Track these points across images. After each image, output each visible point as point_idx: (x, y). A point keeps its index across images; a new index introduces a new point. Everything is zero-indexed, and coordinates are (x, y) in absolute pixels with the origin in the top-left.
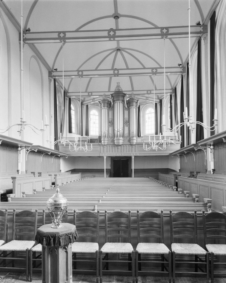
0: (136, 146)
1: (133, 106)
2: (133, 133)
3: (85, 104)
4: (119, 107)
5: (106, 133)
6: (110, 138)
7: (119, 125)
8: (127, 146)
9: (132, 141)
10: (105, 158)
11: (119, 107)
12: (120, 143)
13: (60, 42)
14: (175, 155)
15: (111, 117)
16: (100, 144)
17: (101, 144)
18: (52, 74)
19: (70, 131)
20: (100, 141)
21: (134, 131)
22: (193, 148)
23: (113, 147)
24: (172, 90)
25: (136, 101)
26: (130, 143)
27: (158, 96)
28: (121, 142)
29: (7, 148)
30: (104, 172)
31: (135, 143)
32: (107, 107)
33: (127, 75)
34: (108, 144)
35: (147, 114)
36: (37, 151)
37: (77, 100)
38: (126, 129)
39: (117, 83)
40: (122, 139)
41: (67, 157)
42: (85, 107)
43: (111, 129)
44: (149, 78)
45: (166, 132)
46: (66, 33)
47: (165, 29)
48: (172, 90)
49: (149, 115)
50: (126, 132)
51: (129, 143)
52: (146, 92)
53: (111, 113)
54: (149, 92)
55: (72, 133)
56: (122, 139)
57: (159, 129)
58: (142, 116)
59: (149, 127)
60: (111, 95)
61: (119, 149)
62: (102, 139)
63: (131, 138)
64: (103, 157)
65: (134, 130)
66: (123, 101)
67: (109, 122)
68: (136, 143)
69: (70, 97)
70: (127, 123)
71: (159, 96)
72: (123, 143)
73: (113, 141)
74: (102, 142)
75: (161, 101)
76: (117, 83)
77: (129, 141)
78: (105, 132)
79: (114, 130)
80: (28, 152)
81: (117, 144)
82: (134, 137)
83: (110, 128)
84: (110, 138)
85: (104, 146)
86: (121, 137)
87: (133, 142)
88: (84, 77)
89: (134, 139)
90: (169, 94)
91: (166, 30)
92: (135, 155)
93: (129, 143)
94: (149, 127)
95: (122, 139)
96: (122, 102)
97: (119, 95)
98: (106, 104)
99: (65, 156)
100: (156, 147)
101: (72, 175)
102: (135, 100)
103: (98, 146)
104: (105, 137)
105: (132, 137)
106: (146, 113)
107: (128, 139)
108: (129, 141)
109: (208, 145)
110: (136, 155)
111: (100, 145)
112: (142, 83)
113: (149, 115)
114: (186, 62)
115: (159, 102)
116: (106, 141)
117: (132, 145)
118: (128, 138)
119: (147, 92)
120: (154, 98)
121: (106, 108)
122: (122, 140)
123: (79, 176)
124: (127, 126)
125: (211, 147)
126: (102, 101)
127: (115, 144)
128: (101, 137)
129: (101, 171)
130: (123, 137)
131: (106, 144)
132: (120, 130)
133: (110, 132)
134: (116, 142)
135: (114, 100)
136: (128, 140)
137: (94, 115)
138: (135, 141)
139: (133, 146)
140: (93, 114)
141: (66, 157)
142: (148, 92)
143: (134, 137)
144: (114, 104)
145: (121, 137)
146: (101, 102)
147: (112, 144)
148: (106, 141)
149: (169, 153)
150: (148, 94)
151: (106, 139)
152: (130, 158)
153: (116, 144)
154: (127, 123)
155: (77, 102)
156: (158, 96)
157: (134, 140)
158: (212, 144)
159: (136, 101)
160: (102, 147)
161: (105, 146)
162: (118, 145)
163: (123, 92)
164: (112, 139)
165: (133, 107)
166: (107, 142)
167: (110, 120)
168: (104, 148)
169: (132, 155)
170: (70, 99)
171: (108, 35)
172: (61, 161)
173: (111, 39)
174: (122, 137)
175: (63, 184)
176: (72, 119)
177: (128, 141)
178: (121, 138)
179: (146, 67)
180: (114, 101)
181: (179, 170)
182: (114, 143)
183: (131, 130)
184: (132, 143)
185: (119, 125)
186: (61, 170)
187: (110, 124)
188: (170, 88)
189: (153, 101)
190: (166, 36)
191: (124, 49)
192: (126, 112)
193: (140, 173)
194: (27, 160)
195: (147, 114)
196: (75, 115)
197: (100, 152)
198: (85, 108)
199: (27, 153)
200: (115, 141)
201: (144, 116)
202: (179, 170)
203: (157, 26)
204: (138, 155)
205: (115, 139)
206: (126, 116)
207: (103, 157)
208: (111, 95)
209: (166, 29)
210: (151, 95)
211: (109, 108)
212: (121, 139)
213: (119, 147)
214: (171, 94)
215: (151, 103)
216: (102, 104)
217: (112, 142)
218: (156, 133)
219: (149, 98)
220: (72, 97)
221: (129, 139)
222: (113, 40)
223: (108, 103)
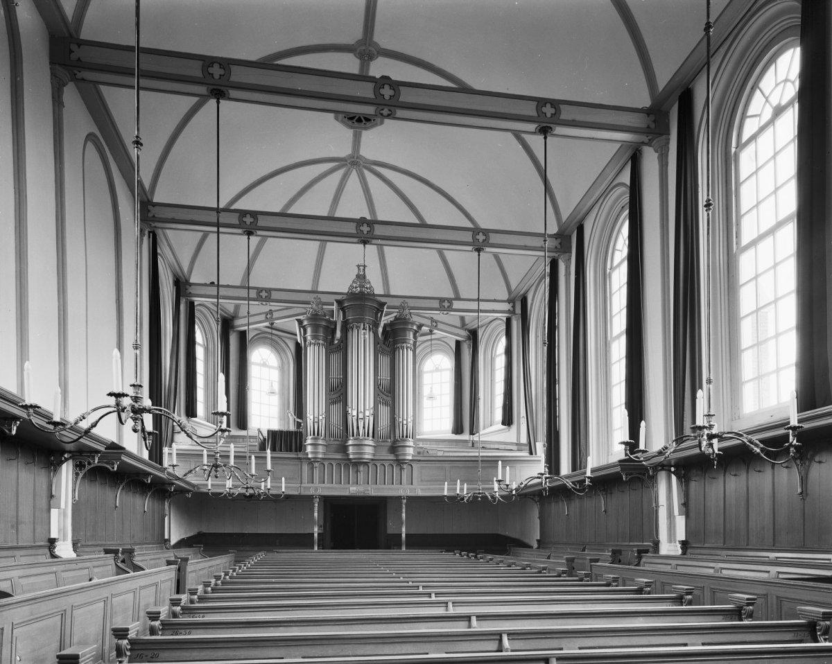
4: (362, 344)
5: (320, 423)
6: (332, 439)
9: (400, 451)
11: (362, 344)
12: (367, 456)
18: (149, 211)
20: (300, 447)
22: (617, 473)
24: (559, 240)
25: (415, 328)
26: (397, 456)
27: (462, 318)
28: (368, 453)
29: (34, 460)
31: (410, 458)
33: (315, 237)
35: (427, 372)
39: (358, 266)
40: (371, 443)
42: (233, 340)
43: (336, 410)
44: (437, 256)
45: (492, 430)
46: (259, 217)
47: (548, 105)
48: (559, 240)
49: (433, 375)
50: (384, 422)
55: (196, 417)
56: (371, 444)
57: (465, 415)
59: (432, 415)
60: (338, 301)
62: (309, 441)
66: (376, 325)
67: (331, 389)
71: (467, 321)
72: (374, 455)
73: (343, 449)
75: (473, 336)
76: (358, 266)
79: (345, 414)
80: (80, 470)
81: (355, 459)
82: (407, 437)
84: (332, 439)
85: (311, 462)
86: (368, 436)
87: (405, 455)
88: (400, 113)
89: (408, 444)
90: (504, 316)
91: (391, 89)
94: (432, 415)
95: (371, 443)
98: (321, 329)
102: (413, 324)
103: (297, 462)
104: (318, 434)
105: (403, 437)
106: (742, 348)
107: (390, 444)
108: (394, 449)
112: (406, 273)
113: (433, 375)
114: (574, 222)
116: (321, 449)
121: (321, 342)
124: (386, 404)
126: (308, 319)
127: (350, 459)
129: (303, 541)
130: (373, 437)
133: (332, 420)
134: (354, 454)
135: (348, 320)
136: (387, 448)
137: (266, 370)
140: (262, 362)
143: (407, 437)
145: (368, 436)
146: (305, 323)
150: (441, 308)
151: (320, 442)
153: (351, 457)
156: (462, 318)
157: (407, 448)
159: (415, 328)
162: (358, 463)
163: (379, 298)
165: (405, 345)
167: (335, 382)
171: (373, 97)
173: (381, 112)
174: (371, 438)
177: (388, 450)
178: (370, 442)
179: (429, 222)
182: (348, 455)
184: (401, 458)
188: (506, 297)
190: (392, 108)
191: (373, 166)
192: (385, 361)
193: (418, 542)
194: (77, 498)
195: (427, 372)
198: (235, 342)
199: (77, 474)
200: (351, 450)
203: (464, 83)
205: (350, 442)
208: (338, 301)
209: (220, 64)
210: (452, 313)
213: (361, 468)
214: (507, 315)
216: (309, 330)
218: (458, 429)
219: (439, 323)
220: (197, 300)
222: (389, 115)
223: (326, 328)
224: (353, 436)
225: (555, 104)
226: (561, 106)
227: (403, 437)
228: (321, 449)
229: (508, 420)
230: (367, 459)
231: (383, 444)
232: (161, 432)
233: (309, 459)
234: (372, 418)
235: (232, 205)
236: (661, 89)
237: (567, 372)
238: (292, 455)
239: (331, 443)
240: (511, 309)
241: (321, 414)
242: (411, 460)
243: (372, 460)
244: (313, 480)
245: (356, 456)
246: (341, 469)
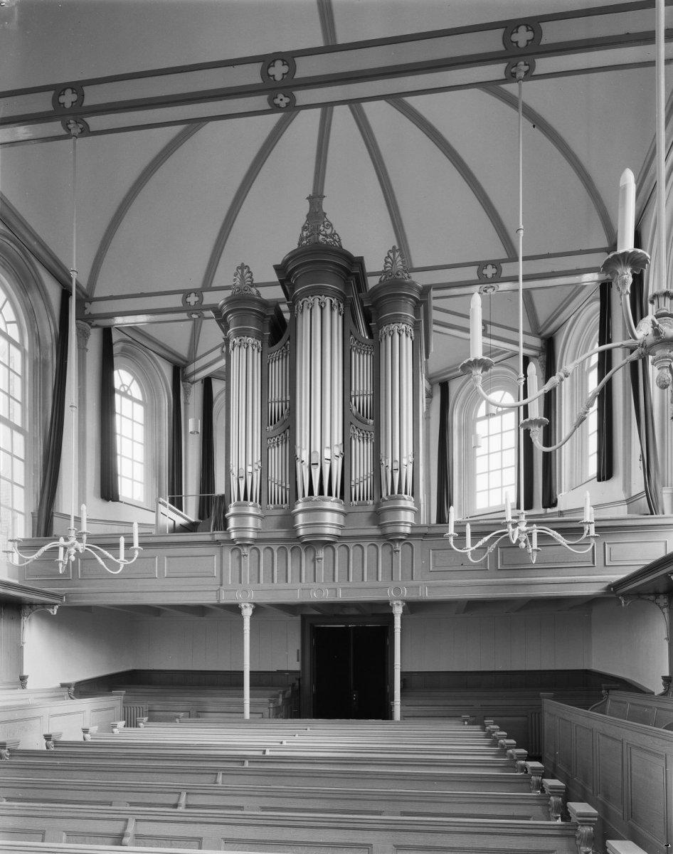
0: (416, 544)
1: (397, 319)
2: (397, 475)
3: (195, 372)
6: (272, 506)
7: (321, 435)
8: (365, 544)
9: (389, 518)
10: (247, 612)
12: (328, 531)
13: (64, 132)
14: (638, 594)
15: (276, 392)
16: (219, 535)
17: (225, 538)
19: (108, 491)
21: (405, 462)
23: (289, 554)
26: (381, 527)
28: (331, 522)
30: (241, 685)
31: (408, 530)
32: (259, 336)
34: (262, 536)
36: (55, 613)
37: (154, 354)
38: (362, 451)
40: (336, 507)
41: (54, 611)
43: (277, 456)
51: (375, 531)
52: (471, 273)
53: (277, 370)
54: (490, 271)
57: (539, 479)
58: (459, 431)
61: (321, 566)
62: (232, 510)
63: (384, 500)
64: (235, 609)
65: (405, 454)
67: (268, 419)
68: (412, 527)
69: (105, 323)
70: (366, 419)
73: (288, 521)
74: (232, 523)
77: (377, 517)
78: (242, 474)
81: (307, 536)
83: (272, 452)
85: (238, 545)
86: (330, 494)
87: (397, 524)
89: (402, 504)
92: (406, 594)
93: (375, 531)
95: (336, 507)
96: (334, 301)
97: (321, 265)
99: (44, 605)
100: (530, 536)
101: (77, 701)
103: (213, 550)
104: (246, 499)
105: (393, 492)
107: (371, 508)
108: (377, 517)
109: (649, 594)
110: (414, 596)
111: (218, 542)
115: (542, 350)
117: (390, 539)
118: (371, 502)
119: (480, 273)
120: (517, 331)
122: (336, 515)
123: (93, 711)
125: (658, 601)
128: (227, 501)
130: (342, 497)
131: (251, 535)
132: (327, 454)
138: (408, 517)
139: (398, 546)
141: (51, 611)
142: (485, 272)
143: (400, 492)
144: (294, 319)
145: (330, 494)
147: (281, 534)
148: (251, 519)
149: (607, 584)
151: (251, 510)
152: (381, 612)
153: (301, 532)
154: (366, 419)
155: (155, 362)
158: (661, 590)
160: (229, 557)
161: (245, 550)
162: (314, 543)
164: (280, 512)
165: (394, 327)
166: (256, 525)
167: (275, 407)
168: (240, 557)
169: (389, 595)
170: (107, 333)
172: (33, 634)
175: (85, 731)
176: (118, 438)
178: (332, 503)
180: (291, 298)
181: (664, 678)
182: (296, 529)
183: (386, 458)
184: (389, 530)
185: (321, 435)
186: (23, 679)
187: (272, 428)
189: (517, 344)
196: (145, 425)
197: (217, 581)
200: (301, 519)
201: (468, 430)
202: (664, 678)
204: (426, 594)
205: (300, 507)
206: (362, 383)
207: (235, 609)
211: (272, 344)
212: (328, 505)
214: (604, 277)
215: (502, 365)
217: (281, 525)
221: (378, 505)
224: (304, 496)
225: (534, 23)
226: (268, 107)
227: (393, 492)
228: (251, 522)
229: (606, 471)
230: (403, 534)
231: (360, 509)
232: (419, 508)
233: (232, 541)
234: (410, 467)
235: (185, 130)
236: (282, 114)
237: (539, 405)
238: (222, 532)
239: (268, 513)
240: (87, 305)
241: (255, 461)
242: (409, 535)
243: (339, 537)
244: (412, 576)
245: (311, 531)
246: (287, 558)
